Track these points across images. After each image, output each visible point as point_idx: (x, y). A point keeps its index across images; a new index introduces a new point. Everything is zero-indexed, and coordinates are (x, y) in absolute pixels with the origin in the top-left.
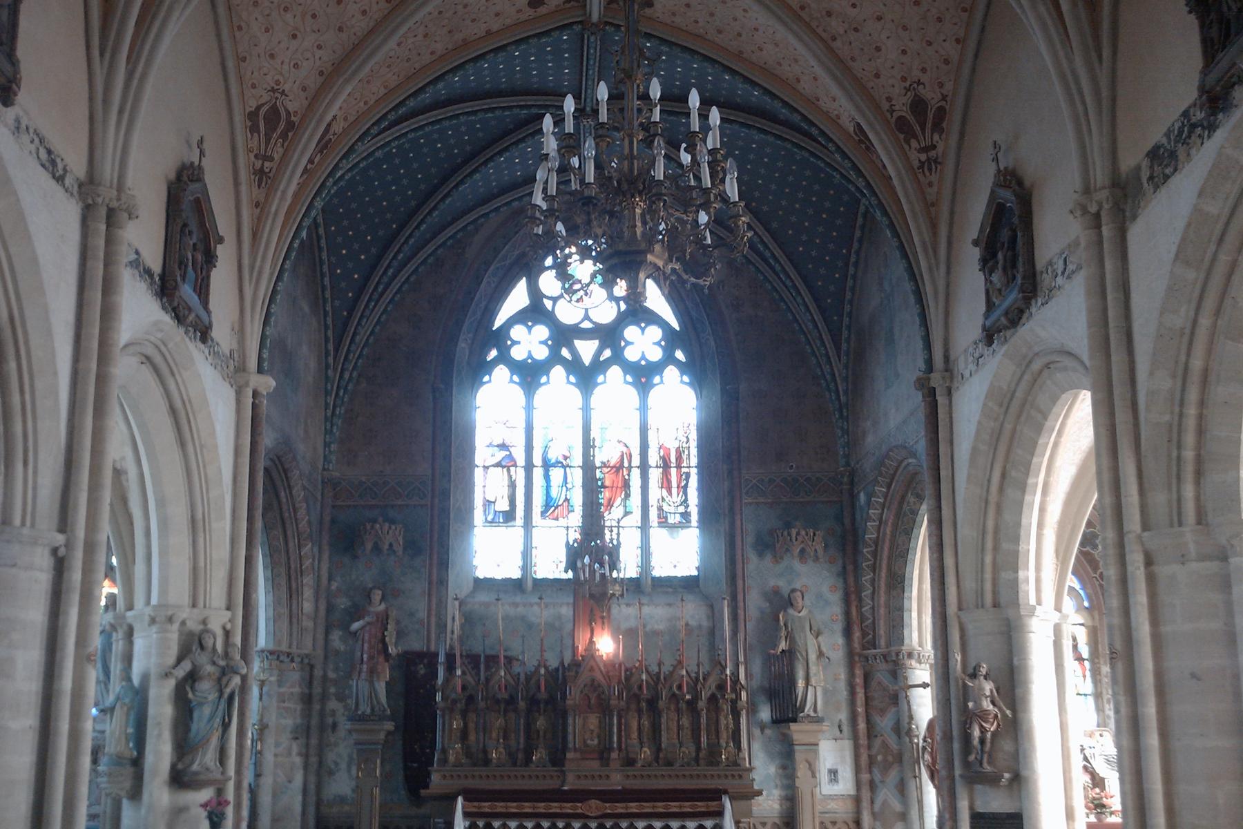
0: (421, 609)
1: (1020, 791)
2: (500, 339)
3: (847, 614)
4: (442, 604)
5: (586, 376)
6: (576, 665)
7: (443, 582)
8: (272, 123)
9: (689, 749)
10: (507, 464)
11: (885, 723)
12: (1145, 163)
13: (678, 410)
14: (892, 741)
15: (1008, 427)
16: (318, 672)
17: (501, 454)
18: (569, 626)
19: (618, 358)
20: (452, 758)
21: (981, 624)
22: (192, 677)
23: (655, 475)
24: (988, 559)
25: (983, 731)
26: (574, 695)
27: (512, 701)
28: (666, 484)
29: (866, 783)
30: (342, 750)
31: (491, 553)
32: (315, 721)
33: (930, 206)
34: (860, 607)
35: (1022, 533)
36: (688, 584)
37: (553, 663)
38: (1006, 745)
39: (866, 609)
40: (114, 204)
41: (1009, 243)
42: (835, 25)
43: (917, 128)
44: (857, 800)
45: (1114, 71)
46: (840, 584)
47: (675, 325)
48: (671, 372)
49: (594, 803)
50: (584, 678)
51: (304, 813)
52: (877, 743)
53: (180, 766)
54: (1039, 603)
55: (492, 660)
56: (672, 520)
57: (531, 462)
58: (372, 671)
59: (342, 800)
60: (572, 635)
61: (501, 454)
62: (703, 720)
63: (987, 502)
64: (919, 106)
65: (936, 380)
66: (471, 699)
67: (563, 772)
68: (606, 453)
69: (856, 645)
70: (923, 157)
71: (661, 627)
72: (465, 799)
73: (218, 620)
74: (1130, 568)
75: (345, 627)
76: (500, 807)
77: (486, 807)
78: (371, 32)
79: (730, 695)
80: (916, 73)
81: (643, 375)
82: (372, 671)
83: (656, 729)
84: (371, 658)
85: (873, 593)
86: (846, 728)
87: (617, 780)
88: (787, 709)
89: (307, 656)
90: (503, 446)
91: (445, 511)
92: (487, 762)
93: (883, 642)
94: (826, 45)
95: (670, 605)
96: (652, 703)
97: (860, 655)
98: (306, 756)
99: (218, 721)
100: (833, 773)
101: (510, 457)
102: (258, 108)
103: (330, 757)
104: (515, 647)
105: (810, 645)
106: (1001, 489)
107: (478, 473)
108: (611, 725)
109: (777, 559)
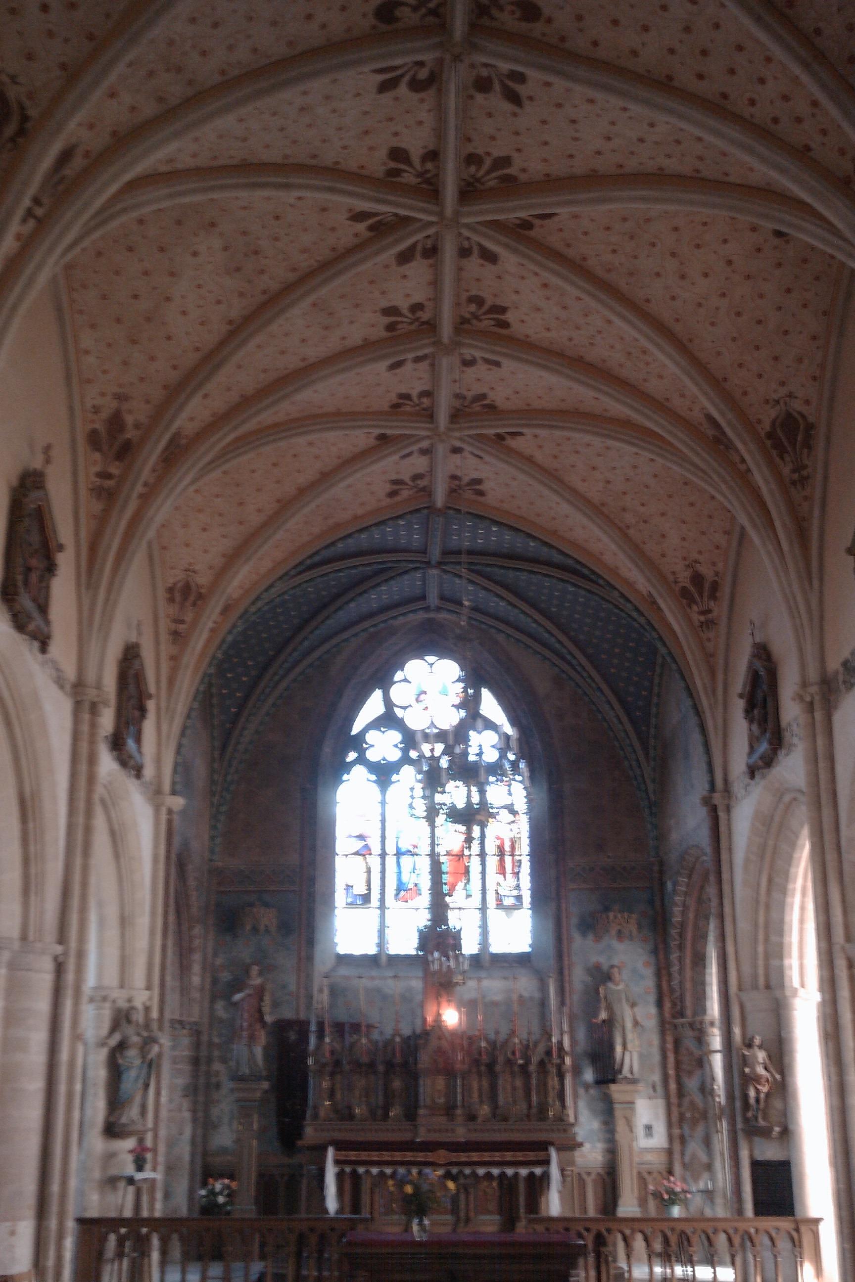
0: (291, 980)
1: (788, 1141)
2: (358, 743)
3: (659, 987)
4: (309, 977)
6: (426, 1034)
7: (310, 958)
8: (186, 595)
9: (522, 1106)
10: (364, 852)
11: (692, 1084)
12: (841, 670)
14: (698, 1099)
15: (771, 843)
16: (205, 1038)
17: (360, 844)
18: (419, 997)
20: (322, 1113)
21: (756, 1001)
22: (122, 1046)
23: (492, 862)
24: (761, 949)
25: (758, 1091)
26: (424, 1059)
27: (372, 1065)
28: (502, 871)
29: (678, 1138)
30: (224, 1106)
31: (351, 932)
32: (202, 1080)
33: (709, 657)
34: (669, 981)
35: (786, 928)
36: (522, 960)
37: (406, 1031)
38: (777, 1104)
39: (675, 983)
40: (96, 699)
41: (762, 701)
42: (629, 518)
43: (696, 596)
44: (670, 1152)
45: (821, 593)
46: (652, 960)
49: (442, 1152)
50: (434, 1043)
51: (192, 1162)
52: (686, 1101)
53: (112, 1119)
54: (803, 985)
55: (356, 1027)
56: (509, 902)
58: (252, 1038)
59: (224, 1151)
60: (422, 1005)
61: (360, 844)
62: (534, 1081)
63: (757, 902)
64: (697, 579)
65: (717, 799)
66: (337, 1063)
67: (415, 1126)
69: (667, 1015)
70: (702, 618)
71: (498, 998)
73: (141, 998)
74: (837, 971)
75: (227, 997)
76: (364, 1156)
77: (353, 1155)
79: (556, 1060)
80: (695, 555)
82: (252, 1038)
83: (493, 1088)
84: (250, 1025)
85: (681, 969)
86: (659, 1089)
87: (461, 1134)
88: (607, 1072)
89: (196, 1023)
90: (361, 837)
92: (351, 1117)
93: (689, 1012)
94: (622, 533)
95: (505, 978)
96: (490, 1066)
97: (669, 1023)
98: (194, 1111)
99: (141, 1081)
100: (649, 1128)
102: (175, 584)
103: (215, 1112)
104: (374, 1016)
105: (627, 1015)
106: (769, 891)
108: (455, 1086)
109: (598, 938)
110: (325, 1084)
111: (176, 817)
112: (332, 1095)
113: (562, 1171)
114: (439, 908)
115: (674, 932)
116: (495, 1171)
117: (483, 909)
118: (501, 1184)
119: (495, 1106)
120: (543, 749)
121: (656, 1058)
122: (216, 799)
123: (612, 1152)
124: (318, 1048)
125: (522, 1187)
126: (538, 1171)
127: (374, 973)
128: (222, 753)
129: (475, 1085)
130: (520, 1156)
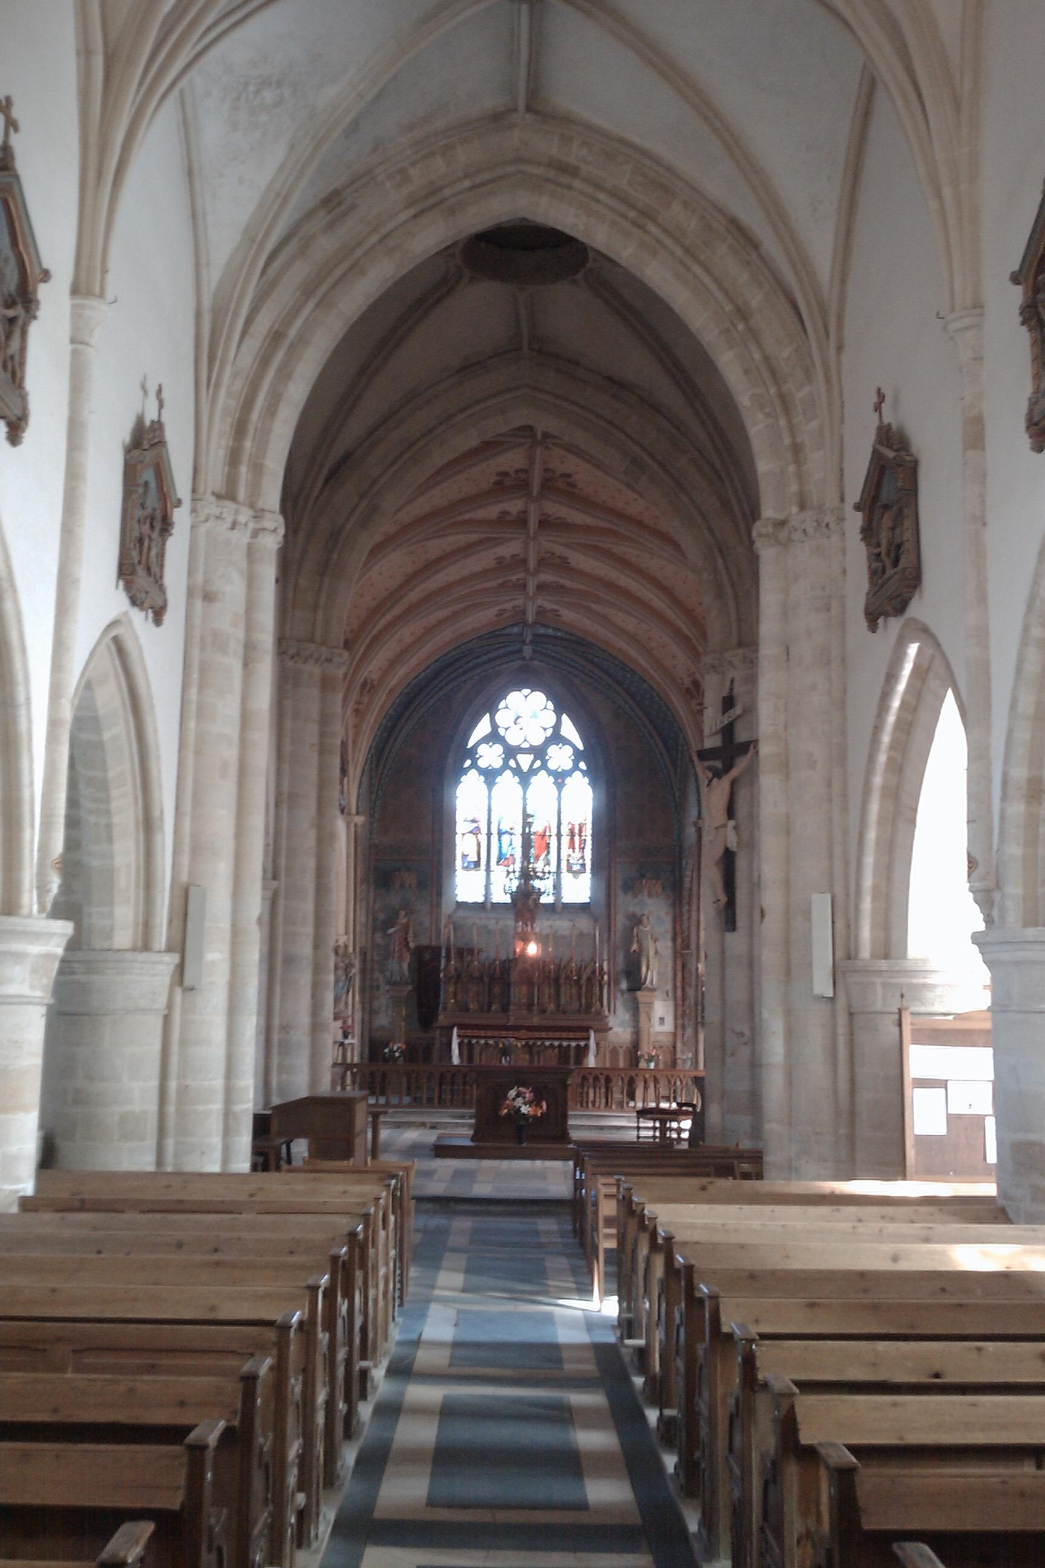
2: (472, 753)
3: (674, 928)
4: (438, 920)
5: (524, 778)
6: (515, 960)
10: (476, 832)
13: (580, 801)
19: (544, 766)
20: (450, 1006)
23: (565, 840)
26: (514, 976)
27: (480, 979)
28: (572, 845)
30: (383, 1001)
31: (467, 887)
34: (681, 925)
36: (583, 907)
37: (504, 958)
39: (685, 926)
44: (675, 1035)
47: (580, 746)
48: (577, 774)
55: (471, 951)
56: (576, 868)
57: (493, 832)
59: (383, 1028)
66: (459, 976)
68: (537, 827)
72: (459, 1028)
77: (469, 1032)
78: (414, 642)
81: (560, 778)
82: (401, 958)
83: (558, 994)
84: (400, 950)
86: (670, 994)
87: (536, 1021)
88: (636, 984)
90: (474, 821)
91: (440, 863)
92: (468, 1010)
96: (557, 981)
100: (662, 1020)
101: (478, 828)
103: (376, 1004)
107: (458, 838)
109: (635, 896)
110: (451, 989)
111: (359, 829)
112: (455, 995)
113: (597, 1044)
114: (527, 875)
115: (685, 893)
116: (556, 1043)
117: (558, 872)
118: (560, 1051)
119: (558, 1005)
120: (605, 759)
121: (670, 974)
122: (373, 797)
123: (637, 1034)
124: (447, 966)
125: (572, 1052)
126: (582, 1044)
127: (482, 915)
128: (377, 765)
129: (547, 991)
130: (571, 1035)
